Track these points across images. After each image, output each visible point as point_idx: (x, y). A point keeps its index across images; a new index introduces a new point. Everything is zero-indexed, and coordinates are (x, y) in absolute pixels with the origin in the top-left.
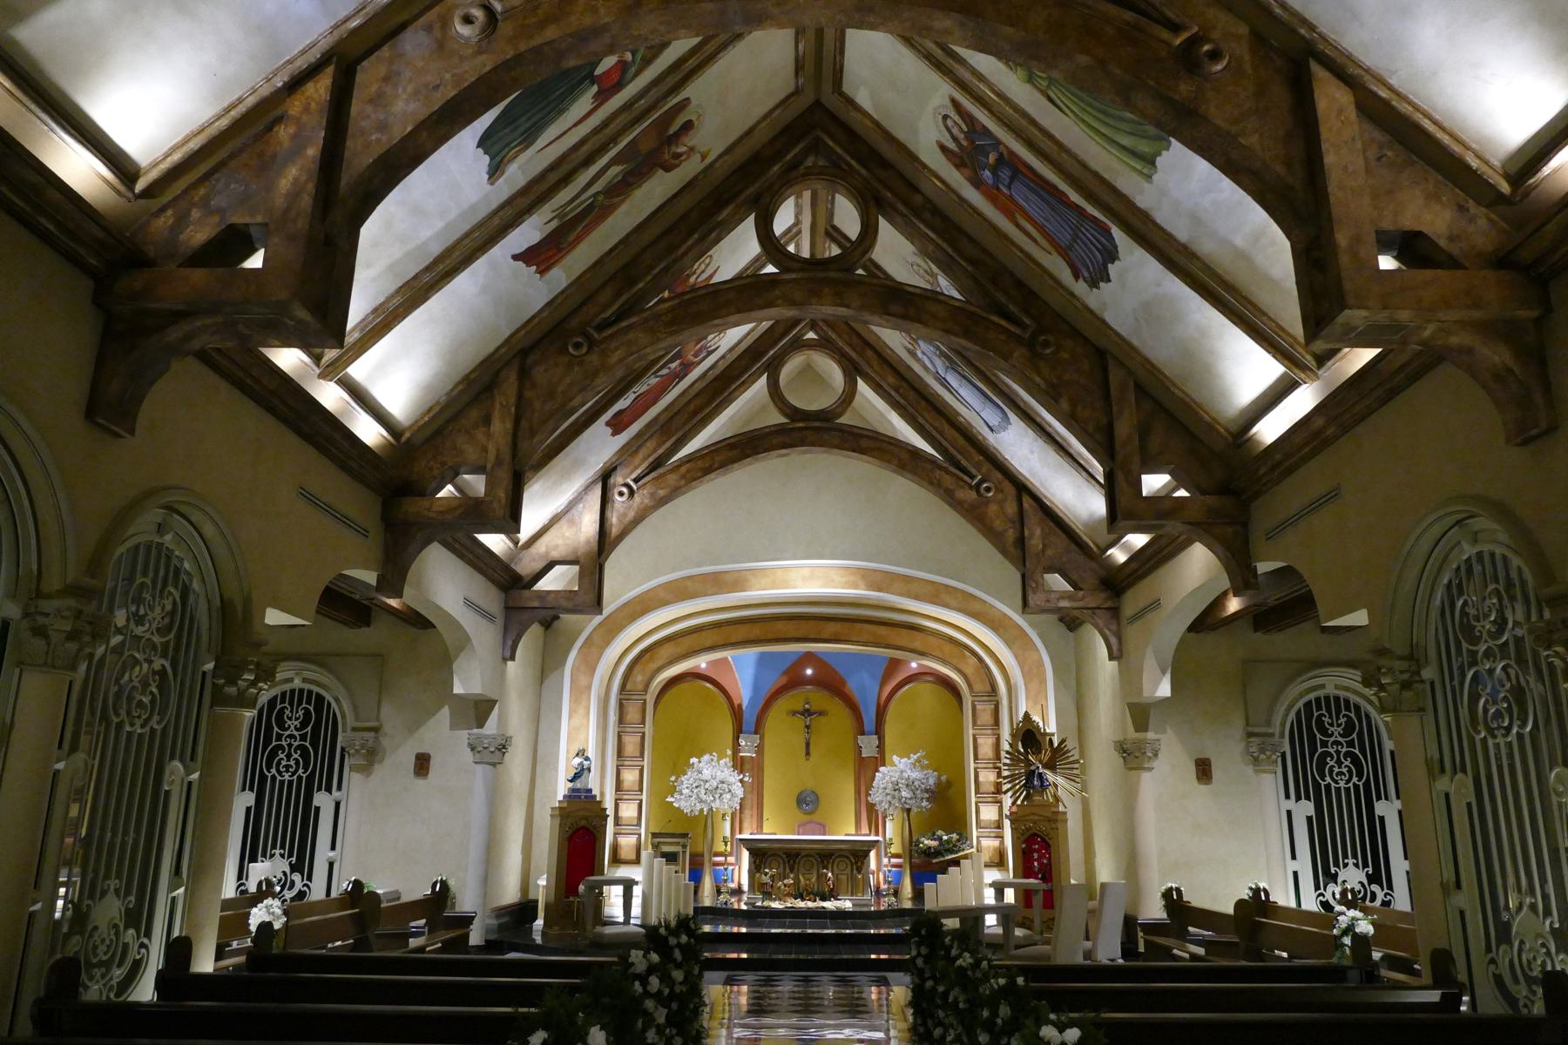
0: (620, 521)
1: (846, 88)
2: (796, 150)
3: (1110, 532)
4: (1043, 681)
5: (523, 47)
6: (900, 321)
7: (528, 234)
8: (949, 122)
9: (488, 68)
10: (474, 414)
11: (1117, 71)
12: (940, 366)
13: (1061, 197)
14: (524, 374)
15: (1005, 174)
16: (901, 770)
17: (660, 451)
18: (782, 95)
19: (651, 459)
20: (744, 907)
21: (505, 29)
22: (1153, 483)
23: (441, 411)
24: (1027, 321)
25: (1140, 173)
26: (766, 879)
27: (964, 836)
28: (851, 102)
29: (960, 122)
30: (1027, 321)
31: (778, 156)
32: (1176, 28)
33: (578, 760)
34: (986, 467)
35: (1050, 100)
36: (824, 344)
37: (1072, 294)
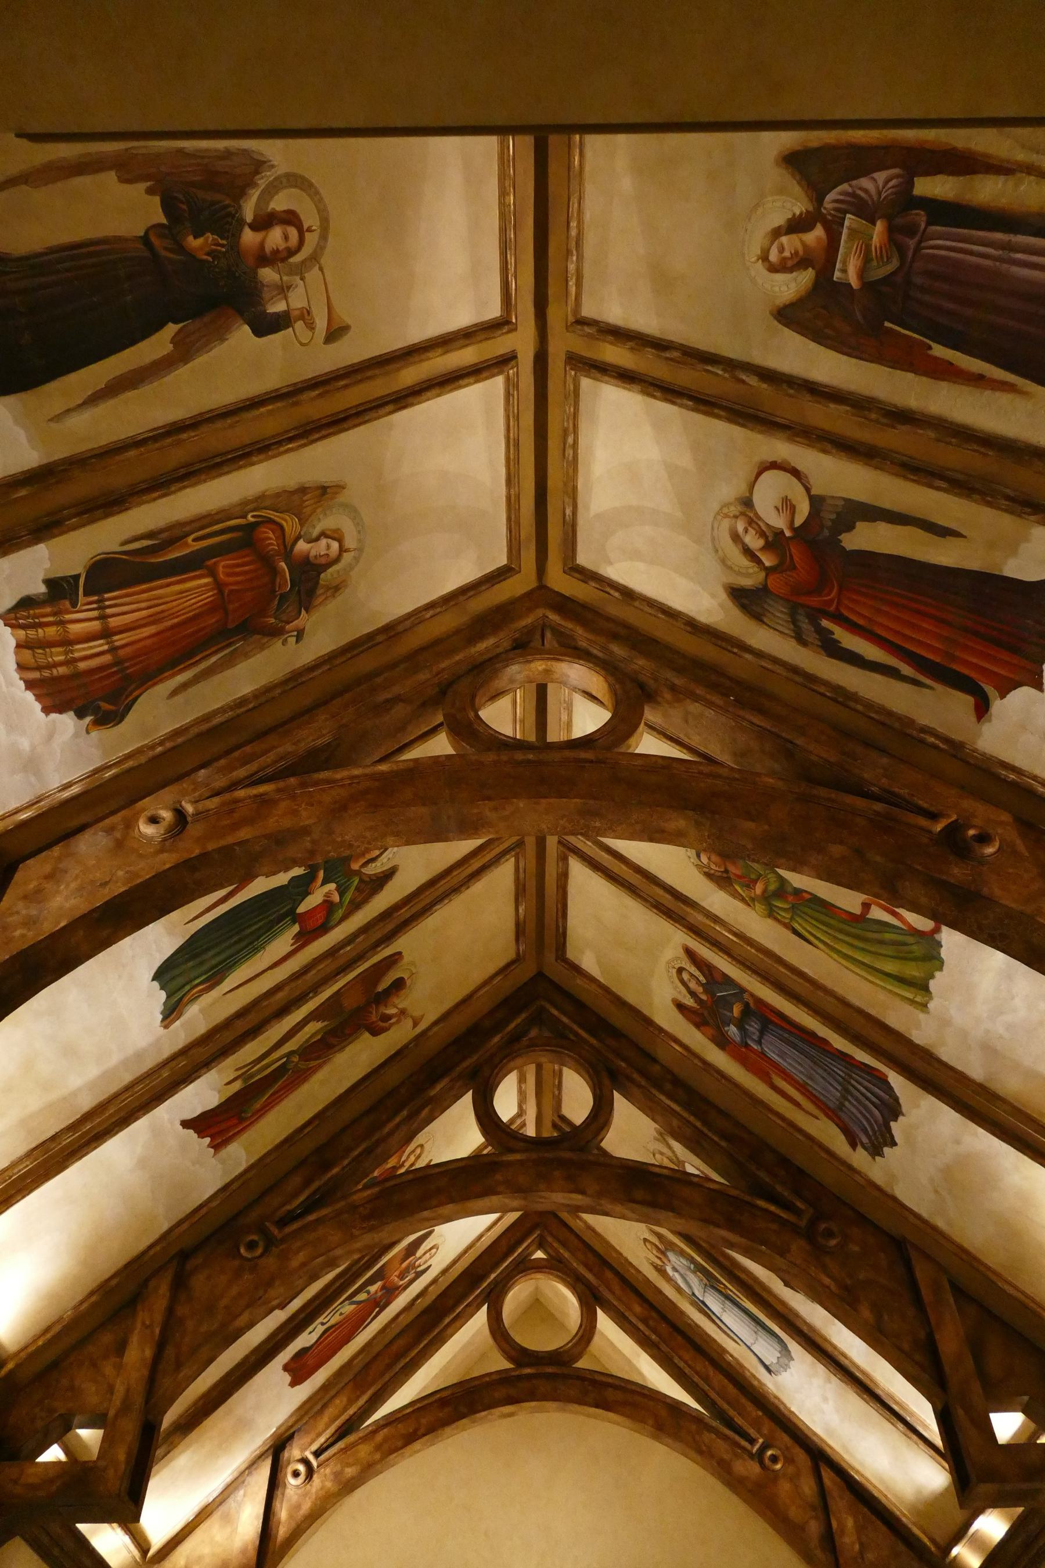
0: (291, 1516)
1: (571, 955)
2: (519, 1020)
3: (962, 1505)
5: (211, 846)
6: (645, 1210)
7: (201, 1095)
8: (685, 976)
9: (168, 866)
10: (107, 1338)
11: (878, 858)
12: (696, 1284)
13: (821, 1044)
14: (180, 1284)
15: (753, 1028)
17: (351, 1411)
18: (502, 963)
19: (338, 1423)
21: (194, 830)
22: (1007, 1425)
23: (57, 1337)
24: (800, 1204)
25: (912, 1002)
28: (576, 969)
29: (697, 973)
30: (800, 1204)
31: (497, 1028)
32: (934, 816)
34: (767, 1426)
35: (795, 932)
36: (556, 1266)
37: (850, 1168)
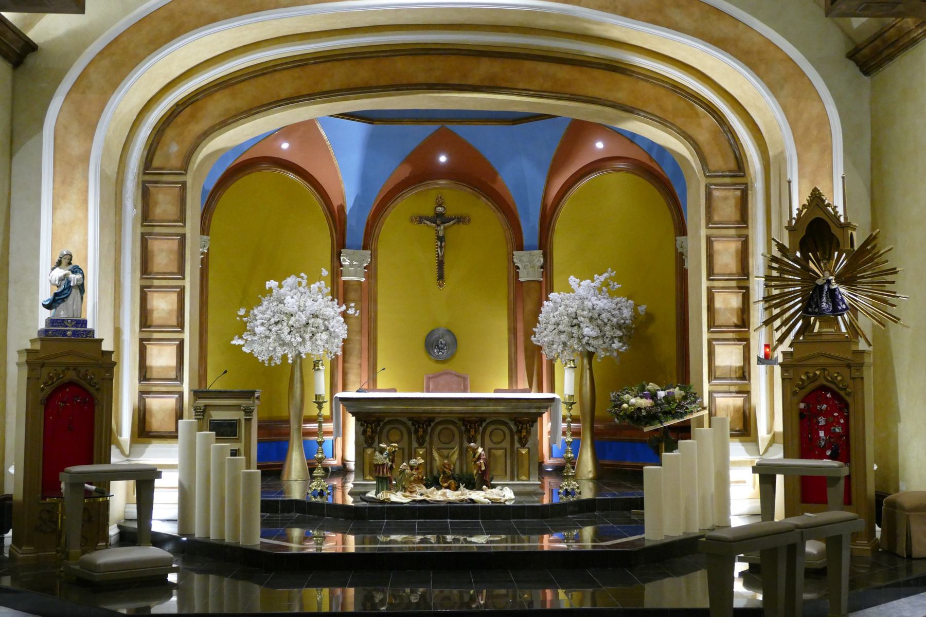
4: (827, 150)
16: (579, 298)
20: (350, 501)
26: (380, 458)
27: (692, 396)
33: (59, 272)
